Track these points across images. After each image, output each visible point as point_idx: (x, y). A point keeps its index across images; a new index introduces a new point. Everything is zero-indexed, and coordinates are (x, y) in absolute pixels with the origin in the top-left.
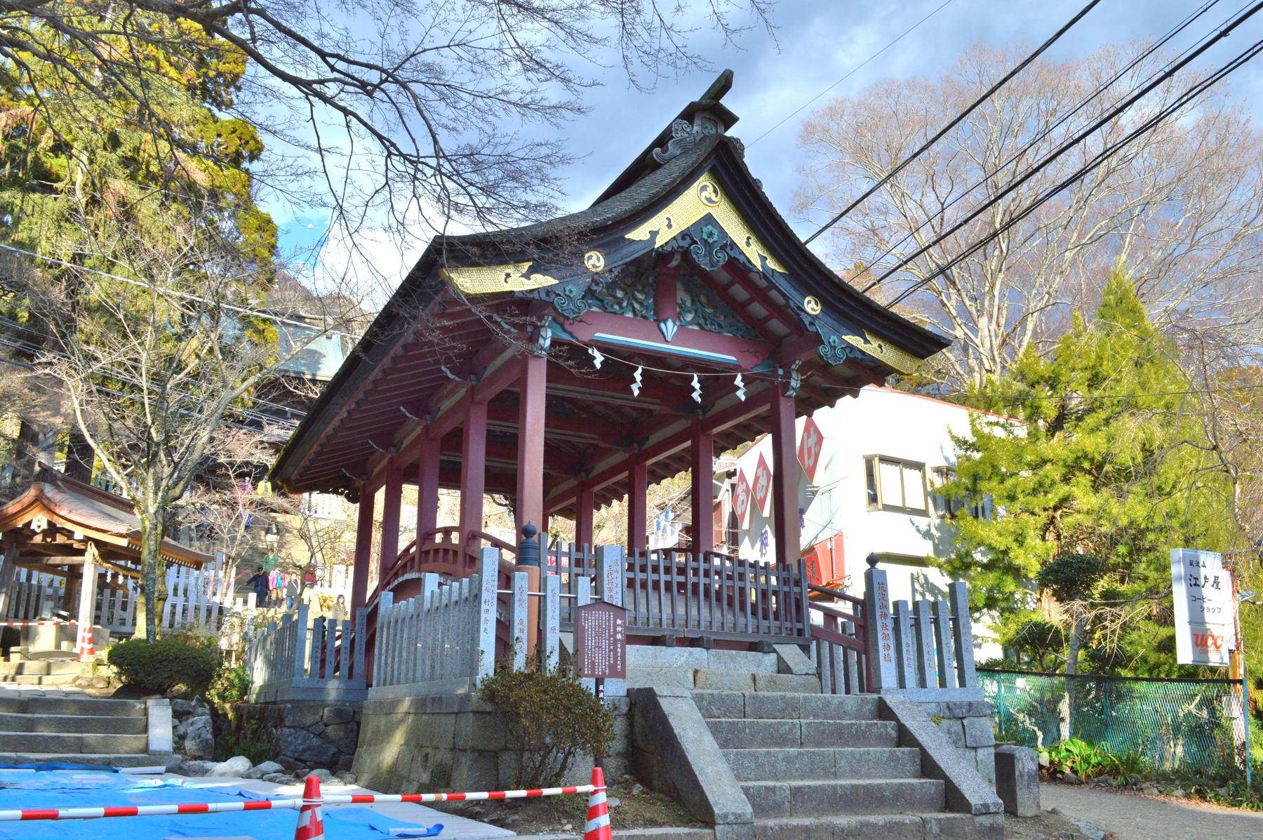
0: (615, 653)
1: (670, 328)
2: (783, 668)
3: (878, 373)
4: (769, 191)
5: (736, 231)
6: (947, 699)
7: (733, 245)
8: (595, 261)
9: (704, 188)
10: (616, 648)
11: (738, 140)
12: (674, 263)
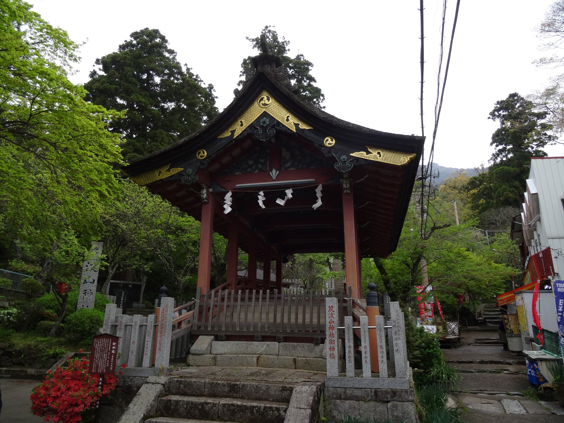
0: (110, 360)
1: (274, 173)
6: (376, 386)
7: (279, 123)
10: (111, 358)
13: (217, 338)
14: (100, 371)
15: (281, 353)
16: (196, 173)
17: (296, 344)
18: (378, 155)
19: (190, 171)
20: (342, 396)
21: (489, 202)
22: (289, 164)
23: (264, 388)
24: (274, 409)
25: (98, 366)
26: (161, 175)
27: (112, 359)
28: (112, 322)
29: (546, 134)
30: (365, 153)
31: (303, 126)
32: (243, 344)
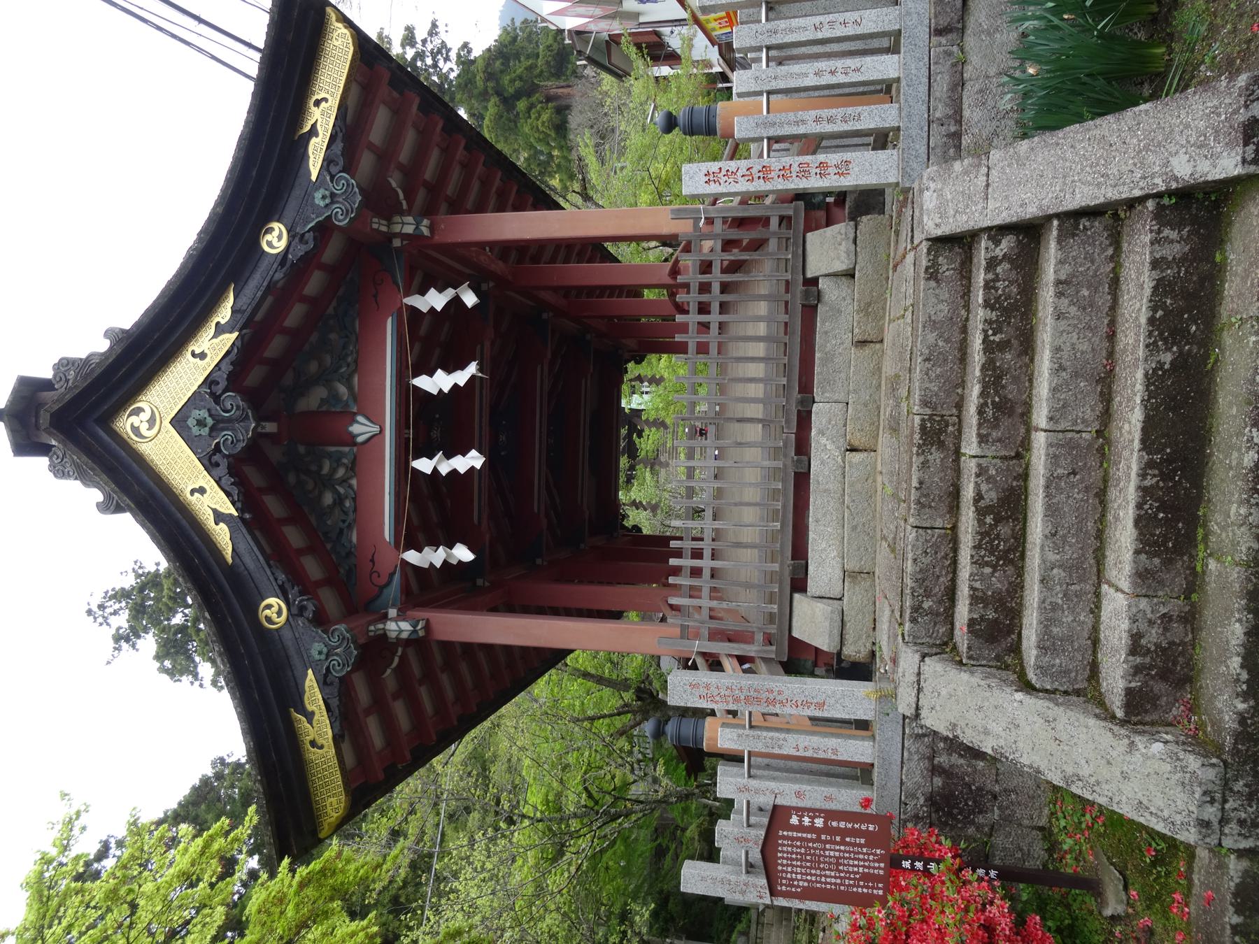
0: (844, 833)
1: (362, 429)
6: (922, 33)
7: (209, 382)
8: (274, 609)
10: (838, 831)
13: (799, 584)
14: (879, 869)
15: (842, 397)
16: (325, 632)
17: (817, 355)
18: (323, 104)
19: (316, 649)
20: (953, 129)
21: (559, 166)
22: (342, 390)
23: (931, 337)
24: (990, 276)
26: (320, 741)
27: (842, 825)
28: (738, 873)
29: (424, 42)
30: (314, 140)
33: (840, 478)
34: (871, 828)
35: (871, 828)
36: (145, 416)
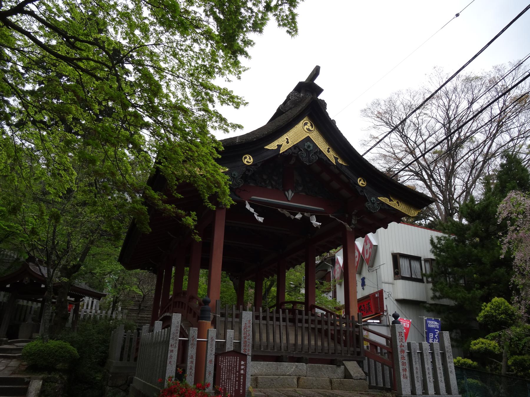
0: (239, 381)
1: (290, 194)
2: (347, 375)
3: (398, 217)
4: (341, 126)
5: (322, 145)
8: (248, 160)
9: (306, 124)
10: (240, 379)
11: (323, 101)
12: (292, 162)
25: (225, 389)
27: (242, 380)
31: (340, 161)
32: (273, 365)
33: (282, 374)
34: (241, 391)
35: (241, 391)
36: (310, 128)
